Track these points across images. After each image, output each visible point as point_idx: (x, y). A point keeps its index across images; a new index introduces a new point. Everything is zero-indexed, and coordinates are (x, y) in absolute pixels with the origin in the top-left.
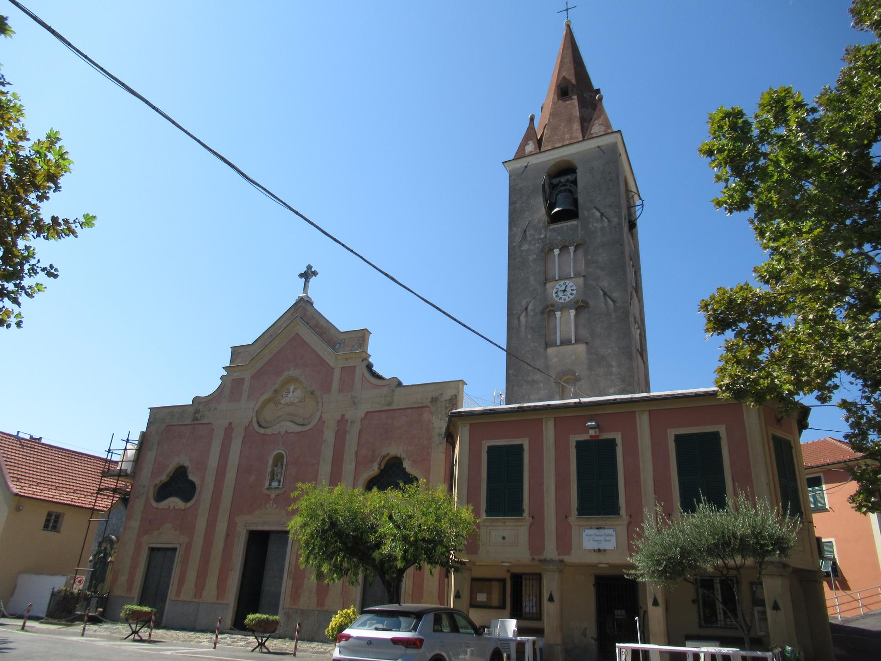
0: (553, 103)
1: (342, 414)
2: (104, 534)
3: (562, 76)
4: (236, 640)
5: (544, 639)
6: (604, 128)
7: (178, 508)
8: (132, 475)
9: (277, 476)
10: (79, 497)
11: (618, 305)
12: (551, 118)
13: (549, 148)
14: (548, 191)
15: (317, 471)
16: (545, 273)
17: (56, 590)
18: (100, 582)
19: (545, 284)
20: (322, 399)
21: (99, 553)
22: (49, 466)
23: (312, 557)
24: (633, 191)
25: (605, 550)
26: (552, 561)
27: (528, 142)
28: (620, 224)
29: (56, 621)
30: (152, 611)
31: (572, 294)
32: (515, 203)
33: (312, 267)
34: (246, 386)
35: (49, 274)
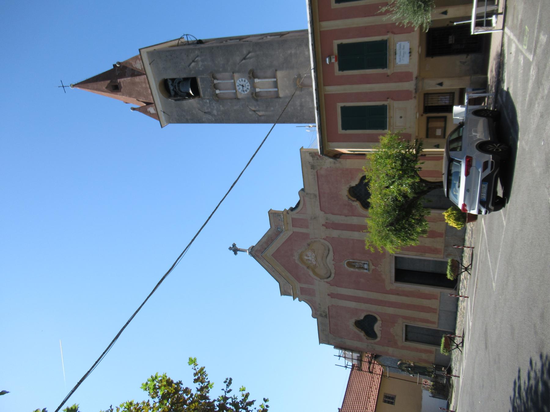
0: (123, 95)
1: (322, 226)
2: (397, 368)
3: (106, 89)
4: (463, 286)
5: (467, 88)
6: (138, 60)
7: (380, 324)
8: (361, 352)
9: (361, 265)
10: (374, 385)
11: (251, 50)
12: (132, 96)
13: (151, 97)
14: (179, 98)
15: (357, 240)
16: (231, 99)
17: (431, 395)
18: (426, 369)
19: (238, 99)
20: (312, 239)
21: (408, 371)
22: (356, 403)
23: (411, 237)
24: (177, 42)
25: (410, 49)
26: (416, 85)
27: (148, 111)
28: (199, 49)
29: (450, 394)
30: (444, 337)
31: (245, 81)
32: (187, 119)
33: (230, 247)
34: (304, 286)
35: (230, 383)
